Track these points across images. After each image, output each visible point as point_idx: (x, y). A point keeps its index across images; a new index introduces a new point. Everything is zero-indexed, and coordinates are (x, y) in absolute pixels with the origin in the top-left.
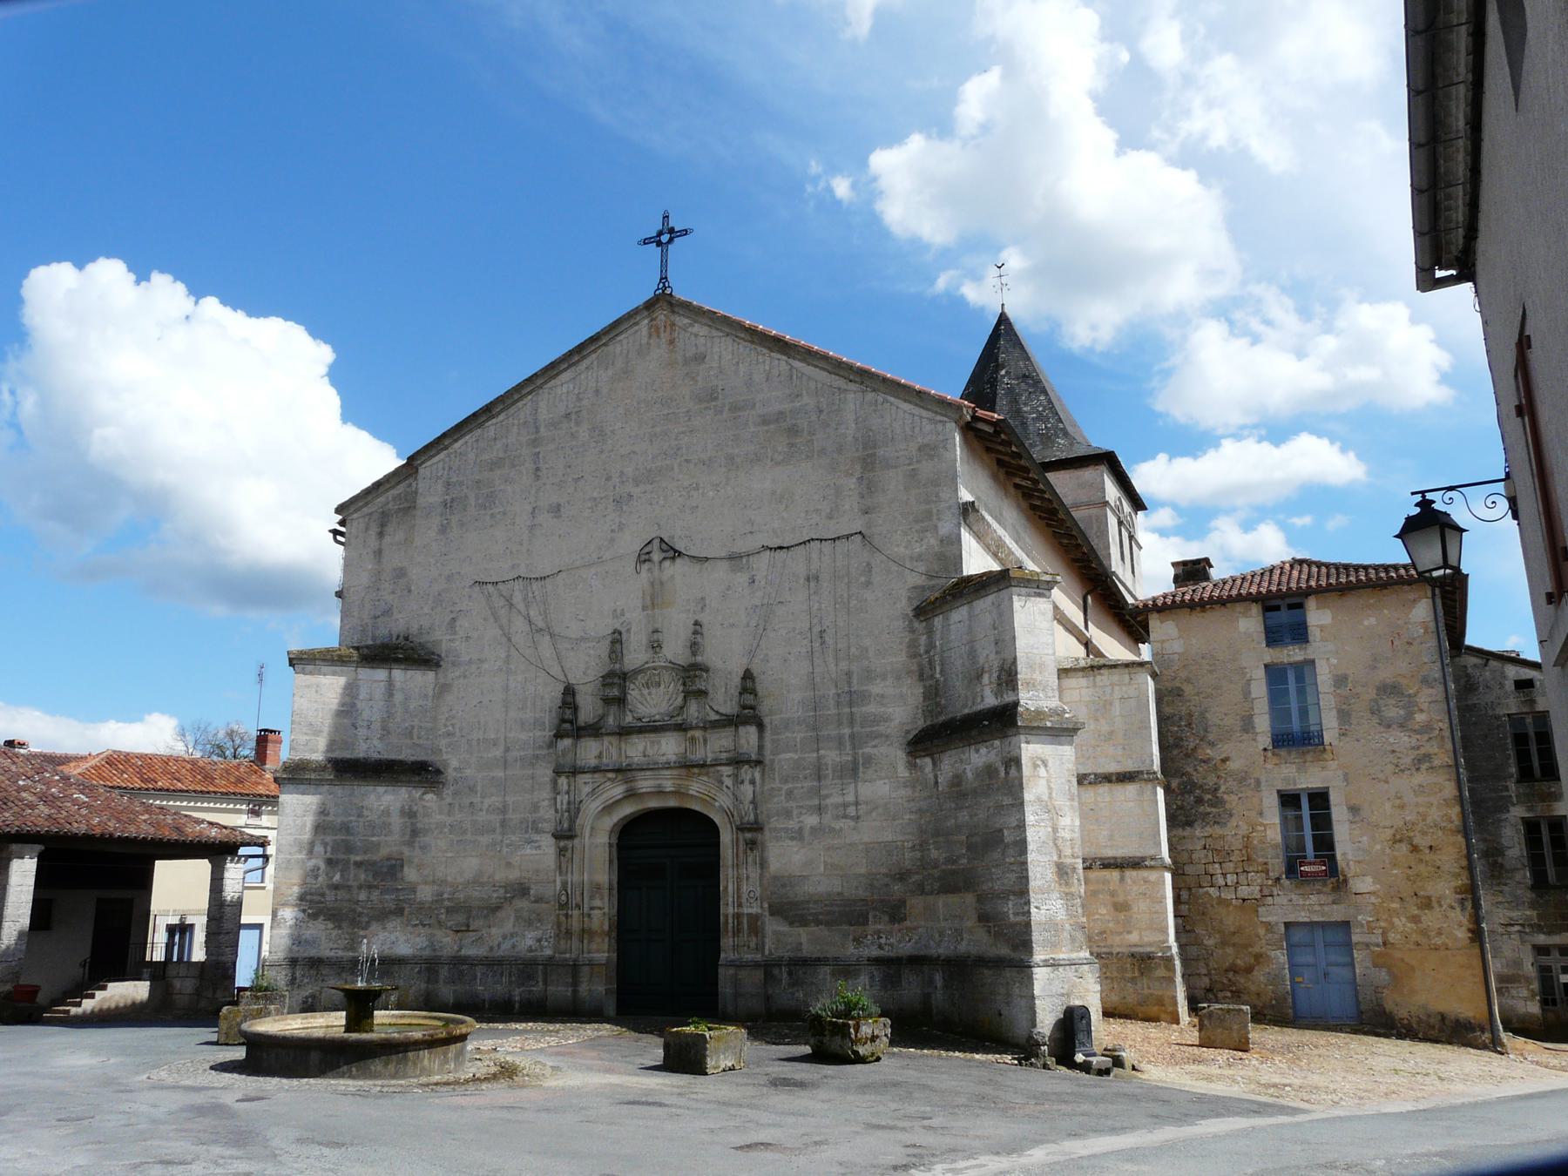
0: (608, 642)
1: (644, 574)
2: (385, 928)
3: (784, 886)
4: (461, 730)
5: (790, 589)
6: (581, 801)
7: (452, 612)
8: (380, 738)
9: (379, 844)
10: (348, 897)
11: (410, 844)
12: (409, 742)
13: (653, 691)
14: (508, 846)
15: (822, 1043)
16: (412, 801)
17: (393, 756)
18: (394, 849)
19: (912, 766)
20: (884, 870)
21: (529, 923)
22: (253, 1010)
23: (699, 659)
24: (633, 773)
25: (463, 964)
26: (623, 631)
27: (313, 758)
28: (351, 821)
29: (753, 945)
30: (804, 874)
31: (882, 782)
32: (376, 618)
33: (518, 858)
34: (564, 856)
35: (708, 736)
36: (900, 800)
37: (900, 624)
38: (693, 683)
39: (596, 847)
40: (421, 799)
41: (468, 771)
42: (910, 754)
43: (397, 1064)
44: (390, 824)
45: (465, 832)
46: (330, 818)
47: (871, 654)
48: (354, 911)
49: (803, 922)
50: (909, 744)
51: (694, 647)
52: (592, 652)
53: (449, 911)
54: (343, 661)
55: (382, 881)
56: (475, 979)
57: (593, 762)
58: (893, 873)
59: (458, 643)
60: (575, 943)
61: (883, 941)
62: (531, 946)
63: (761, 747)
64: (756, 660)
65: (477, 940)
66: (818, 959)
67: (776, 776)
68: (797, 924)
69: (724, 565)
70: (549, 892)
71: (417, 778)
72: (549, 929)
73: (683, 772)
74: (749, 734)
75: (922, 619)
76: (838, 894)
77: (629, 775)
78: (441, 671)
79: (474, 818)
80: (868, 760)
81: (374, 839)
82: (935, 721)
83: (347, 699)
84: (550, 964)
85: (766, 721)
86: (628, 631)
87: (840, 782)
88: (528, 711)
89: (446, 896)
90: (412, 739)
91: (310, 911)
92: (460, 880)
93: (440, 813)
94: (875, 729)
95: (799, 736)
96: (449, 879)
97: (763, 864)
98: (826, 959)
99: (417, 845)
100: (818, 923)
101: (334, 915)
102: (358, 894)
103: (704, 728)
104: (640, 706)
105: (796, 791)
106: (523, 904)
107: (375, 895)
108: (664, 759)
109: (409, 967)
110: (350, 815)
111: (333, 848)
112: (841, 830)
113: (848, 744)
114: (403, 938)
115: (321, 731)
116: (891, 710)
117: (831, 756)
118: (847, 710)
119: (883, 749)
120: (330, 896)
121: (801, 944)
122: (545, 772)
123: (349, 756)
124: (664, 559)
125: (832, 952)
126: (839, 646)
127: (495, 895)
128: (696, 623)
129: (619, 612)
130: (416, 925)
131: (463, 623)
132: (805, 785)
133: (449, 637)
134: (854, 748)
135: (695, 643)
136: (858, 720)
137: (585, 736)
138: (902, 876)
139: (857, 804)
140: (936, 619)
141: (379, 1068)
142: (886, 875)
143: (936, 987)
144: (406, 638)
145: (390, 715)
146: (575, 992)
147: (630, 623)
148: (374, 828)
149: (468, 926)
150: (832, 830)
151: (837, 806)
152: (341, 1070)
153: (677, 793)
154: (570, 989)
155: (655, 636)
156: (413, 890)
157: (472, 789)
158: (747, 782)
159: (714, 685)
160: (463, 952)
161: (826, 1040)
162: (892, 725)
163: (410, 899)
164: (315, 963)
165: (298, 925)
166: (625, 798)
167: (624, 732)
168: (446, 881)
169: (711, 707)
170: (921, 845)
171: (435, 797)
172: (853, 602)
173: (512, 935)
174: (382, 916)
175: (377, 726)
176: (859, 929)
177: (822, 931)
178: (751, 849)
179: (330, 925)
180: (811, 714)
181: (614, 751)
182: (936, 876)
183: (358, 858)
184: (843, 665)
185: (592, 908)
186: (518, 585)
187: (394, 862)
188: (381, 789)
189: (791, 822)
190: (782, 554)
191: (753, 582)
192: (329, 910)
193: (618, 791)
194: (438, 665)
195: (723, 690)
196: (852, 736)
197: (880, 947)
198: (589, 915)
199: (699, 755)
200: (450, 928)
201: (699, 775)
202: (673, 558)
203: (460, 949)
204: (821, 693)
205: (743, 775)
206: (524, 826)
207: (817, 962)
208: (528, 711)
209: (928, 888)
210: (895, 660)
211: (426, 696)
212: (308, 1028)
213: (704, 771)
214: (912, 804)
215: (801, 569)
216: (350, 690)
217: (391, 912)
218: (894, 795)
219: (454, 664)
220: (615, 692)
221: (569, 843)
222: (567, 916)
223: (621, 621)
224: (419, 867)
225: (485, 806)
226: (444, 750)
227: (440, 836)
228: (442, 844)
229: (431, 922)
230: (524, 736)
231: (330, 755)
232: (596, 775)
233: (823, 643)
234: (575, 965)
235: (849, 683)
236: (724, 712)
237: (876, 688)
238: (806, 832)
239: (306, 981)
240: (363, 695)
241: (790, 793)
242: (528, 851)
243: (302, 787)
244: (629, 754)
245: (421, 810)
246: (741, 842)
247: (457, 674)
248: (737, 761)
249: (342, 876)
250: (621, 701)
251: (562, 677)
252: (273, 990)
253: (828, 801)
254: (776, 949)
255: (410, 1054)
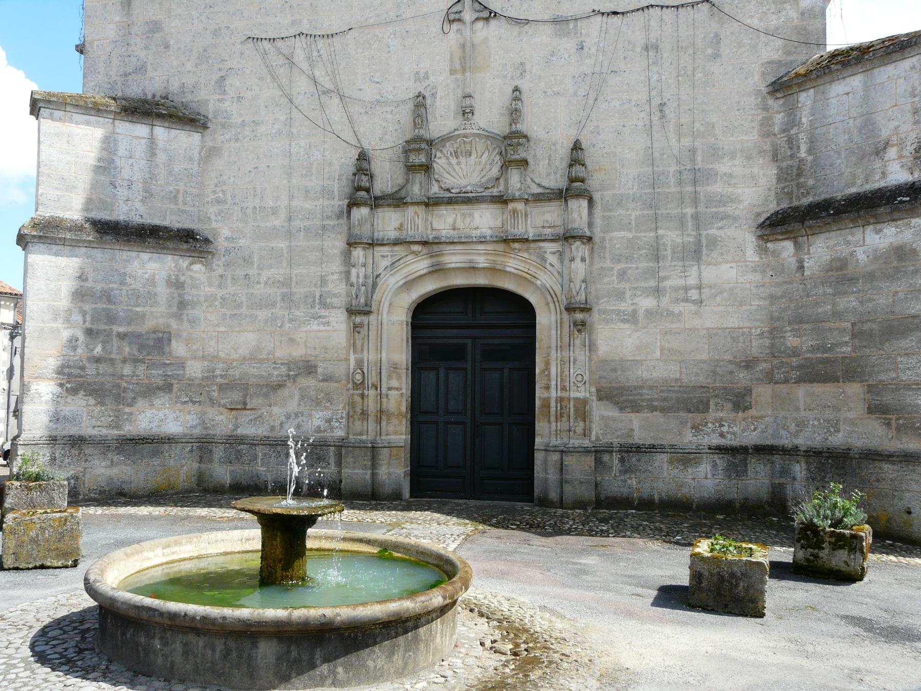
0: (410, 105)
1: (452, 35)
2: (152, 405)
3: (614, 370)
4: (234, 196)
5: (625, 58)
6: (378, 276)
7: (220, 70)
8: (142, 201)
9: (144, 315)
10: (110, 370)
11: (178, 317)
12: (173, 206)
13: (463, 160)
14: (291, 321)
15: (816, 556)
16: (179, 271)
17: (157, 221)
18: (161, 321)
19: (762, 250)
20: (728, 357)
21: (317, 403)
22: (54, 520)
23: (519, 127)
24: (440, 246)
25: (239, 444)
26: (427, 95)
27: (66, 216)
28: (112, 290)
29: (579, 430)
30: (638, 358)
31: (729, 265)
32: (126, 75)
33: (302, 335)
34: (359, 332)
35: (528, 209)
36: (748, 286)
37: (752, 101)
38: (515, 151)
39: (393, 324)
40: (188, 269)
41: (242, 242)
42: (760, 237)
43: (406, 651)
44: (156, 294)
45: (239, 306)
46: (89, 284)
47: (717, 131)
48: (118, 386)
49: (635, 407)
50: (761, 226)
51: (515, 114)
52: (390, 116)
53: (222, 388)
54: (99, 110)
55: (148, 354)
56: (256, 459)
57: (393, 234)
58: (738, 360)
59: (227, 104)
60: (371, 425)
61: (725, 429)
62: (319, 427)
63: (590, 225)
64: (585, 132)
65: (256, 419)
66: (653, 447)
67: (607, 255)
68: (628, 410)
69: (548, 29)
70: (339, 370)
71: (185, 246)
72: (340, 409)
73: (501, 247)
74: (579, 207)
75: (780, 95)
76: (676, 380)
77: (436, 248)
78: (208, 132)
79: (251, 291)
80: (713, 242)
81: (138, 309)
82: (795, 203)
83: (105, 154)
84: (342, 447)
85: (596, 196)
86: (433, 95)
87: (681, 263)
88: (313, 178)
89: (218, 372)
90: (177, 204)
91: (69, 386)
92: (234, 356)
93: (210, 285)
94: (722, 209)
95: (634, 214)
96: (222, 355)
97: (591, 347)
98: (662, 447)
99: (185, 317)
100: (653, 409)
101: (94, 390)
102: (122, 368)
103: (527, 201)
104: (446, 175)
105: (629, 272)
106: (309, 382)
107: (141, 369)
108: (477, 233)
109: (180, 446)
110: (111, 282)
111: (93, 317)
112: (680, 314)
113: (690, 224)
114: (171, 416)
115: (74, 187)
116: (740, 191)
117: (671, 236)
118: (689, 188)
119: (730, 232)
120: (91, 370)
121: (632, 430)
122: (336, 244)
123: (108, 218)
124: (477, 19)
125: (667, 439)
126: (683, 121)
127: (276, 373)
128: (516, 89)
129: (421, 75)
130: (185, 402)
131: (234, 83)
132: (641, 265)
133: (217, 97)
134: (698, 228)
135: (516, 110)
136: (702, 199)
137: (382, 206)
138: (749, 364)
139: (700, 288)
140: (803, 97)
141: (380, 663)
142: (730, 362)
143: (794, 479)
144: (166, 98)
145: (153, 176)
146: (373, 475)
147: (435, 88)
148: (138, 297)
149: (245, 404)
150: (670, 314)
151: (676, 289)
152: (317, 672)
153: (493, 270)
154: (369, 472)
155: (468, 102)
156: (182, 366)
157: (247, 261)
158: (578, 260)
159: (535, 156)
160: (239, 431)
161: (824, 554)
162: (741, 207)
163: (178, 375)
164: (77, 442)
165: (57, 400)
166: (431, 273)
167: (431, 203)
168: (217, 357)
169: (532, 180)
170: (771, 333)
171: (203, 268)
172: (699, 75)
173: (297, 415)
174: (149, 392)
175: (138, 186)
176: (698, 417)
177: (657, 418)
178: (579, 331)
179: (92, 401)
180: (648, 191)
181: (420, 222)
182: (794, 364)
183: (122, 329)
184: (686, 141)
185: (389, 389)
186: (300, 43)
187: (160, 335)
188: (145, 256)
189: (623, 304)
190: (616, 19)
191: (582, 48)
192: (89, 384)
193: (421, 265)
194: (205, 127)
195: (547, 161)
196: (696, 217)
197: (722, 435)
198: (387, 396)
199: (519, 230)
200: (224, 406)
201: (519, 250)
202: (487, 19)
203: (237, 427)
204: (661, 169)
205: (574, 253)
206: (310, 300)
207: (653, 449)
208: (313, 178)
209: (778, 376)
210: (746, 138)
211: (191, 159)
212: (173, 562)
213: (525, 246)
214: (762, 289)
215: (639, 38)
216: (109, 144)
217: (158, 388)
218: (741, 280)
219: (223, 126)
220: (422, 159)
221: (364, 319)
222: (363, 396)
223: (425, 85)
224: (188, 341)
225: (263, 279)
226: (213, 218)
227: (210, 310)
228: (213, 317)
229: (202, 399)
230: (308, 205)
231: (86, 215)
232: (397, 248)
233: (663, 117)
234: (373, 447)
235: (693, 160)
236: (547, 185)
237: (723, 167)
238: (641, 313)
239: (66, 461)
240: (121, 151)
241: (622, 275)
242: (315, 327)
243: (55, 248)
244: (435, 226)
245: (189, 281)
246: (566, 325)
247: (227, 137)
248: (568, 237)
249: (104, 348)
250: (427, 168)
251: (354, 141)
252: (49, 479)
253: (667, 283)
254: (603, 434)
255: (422, 631)
